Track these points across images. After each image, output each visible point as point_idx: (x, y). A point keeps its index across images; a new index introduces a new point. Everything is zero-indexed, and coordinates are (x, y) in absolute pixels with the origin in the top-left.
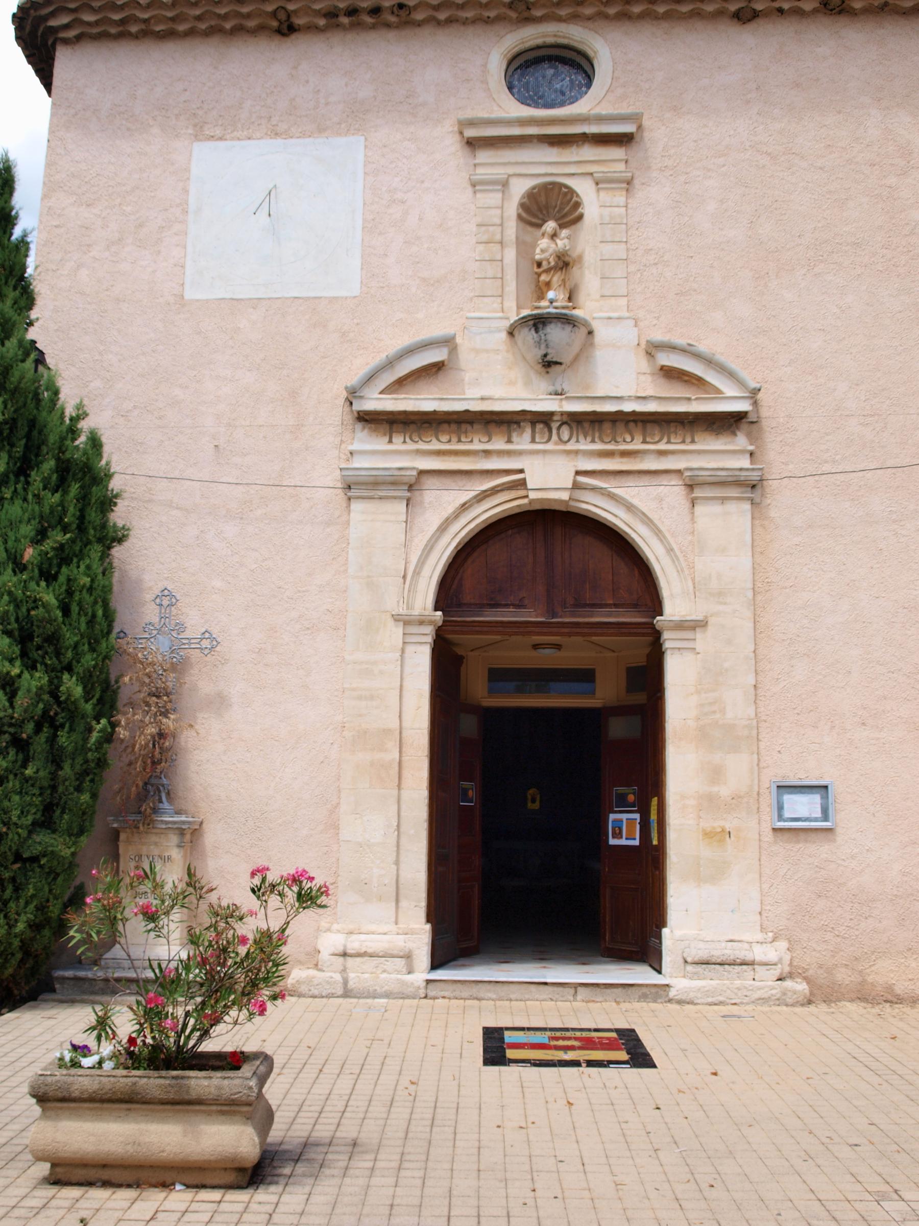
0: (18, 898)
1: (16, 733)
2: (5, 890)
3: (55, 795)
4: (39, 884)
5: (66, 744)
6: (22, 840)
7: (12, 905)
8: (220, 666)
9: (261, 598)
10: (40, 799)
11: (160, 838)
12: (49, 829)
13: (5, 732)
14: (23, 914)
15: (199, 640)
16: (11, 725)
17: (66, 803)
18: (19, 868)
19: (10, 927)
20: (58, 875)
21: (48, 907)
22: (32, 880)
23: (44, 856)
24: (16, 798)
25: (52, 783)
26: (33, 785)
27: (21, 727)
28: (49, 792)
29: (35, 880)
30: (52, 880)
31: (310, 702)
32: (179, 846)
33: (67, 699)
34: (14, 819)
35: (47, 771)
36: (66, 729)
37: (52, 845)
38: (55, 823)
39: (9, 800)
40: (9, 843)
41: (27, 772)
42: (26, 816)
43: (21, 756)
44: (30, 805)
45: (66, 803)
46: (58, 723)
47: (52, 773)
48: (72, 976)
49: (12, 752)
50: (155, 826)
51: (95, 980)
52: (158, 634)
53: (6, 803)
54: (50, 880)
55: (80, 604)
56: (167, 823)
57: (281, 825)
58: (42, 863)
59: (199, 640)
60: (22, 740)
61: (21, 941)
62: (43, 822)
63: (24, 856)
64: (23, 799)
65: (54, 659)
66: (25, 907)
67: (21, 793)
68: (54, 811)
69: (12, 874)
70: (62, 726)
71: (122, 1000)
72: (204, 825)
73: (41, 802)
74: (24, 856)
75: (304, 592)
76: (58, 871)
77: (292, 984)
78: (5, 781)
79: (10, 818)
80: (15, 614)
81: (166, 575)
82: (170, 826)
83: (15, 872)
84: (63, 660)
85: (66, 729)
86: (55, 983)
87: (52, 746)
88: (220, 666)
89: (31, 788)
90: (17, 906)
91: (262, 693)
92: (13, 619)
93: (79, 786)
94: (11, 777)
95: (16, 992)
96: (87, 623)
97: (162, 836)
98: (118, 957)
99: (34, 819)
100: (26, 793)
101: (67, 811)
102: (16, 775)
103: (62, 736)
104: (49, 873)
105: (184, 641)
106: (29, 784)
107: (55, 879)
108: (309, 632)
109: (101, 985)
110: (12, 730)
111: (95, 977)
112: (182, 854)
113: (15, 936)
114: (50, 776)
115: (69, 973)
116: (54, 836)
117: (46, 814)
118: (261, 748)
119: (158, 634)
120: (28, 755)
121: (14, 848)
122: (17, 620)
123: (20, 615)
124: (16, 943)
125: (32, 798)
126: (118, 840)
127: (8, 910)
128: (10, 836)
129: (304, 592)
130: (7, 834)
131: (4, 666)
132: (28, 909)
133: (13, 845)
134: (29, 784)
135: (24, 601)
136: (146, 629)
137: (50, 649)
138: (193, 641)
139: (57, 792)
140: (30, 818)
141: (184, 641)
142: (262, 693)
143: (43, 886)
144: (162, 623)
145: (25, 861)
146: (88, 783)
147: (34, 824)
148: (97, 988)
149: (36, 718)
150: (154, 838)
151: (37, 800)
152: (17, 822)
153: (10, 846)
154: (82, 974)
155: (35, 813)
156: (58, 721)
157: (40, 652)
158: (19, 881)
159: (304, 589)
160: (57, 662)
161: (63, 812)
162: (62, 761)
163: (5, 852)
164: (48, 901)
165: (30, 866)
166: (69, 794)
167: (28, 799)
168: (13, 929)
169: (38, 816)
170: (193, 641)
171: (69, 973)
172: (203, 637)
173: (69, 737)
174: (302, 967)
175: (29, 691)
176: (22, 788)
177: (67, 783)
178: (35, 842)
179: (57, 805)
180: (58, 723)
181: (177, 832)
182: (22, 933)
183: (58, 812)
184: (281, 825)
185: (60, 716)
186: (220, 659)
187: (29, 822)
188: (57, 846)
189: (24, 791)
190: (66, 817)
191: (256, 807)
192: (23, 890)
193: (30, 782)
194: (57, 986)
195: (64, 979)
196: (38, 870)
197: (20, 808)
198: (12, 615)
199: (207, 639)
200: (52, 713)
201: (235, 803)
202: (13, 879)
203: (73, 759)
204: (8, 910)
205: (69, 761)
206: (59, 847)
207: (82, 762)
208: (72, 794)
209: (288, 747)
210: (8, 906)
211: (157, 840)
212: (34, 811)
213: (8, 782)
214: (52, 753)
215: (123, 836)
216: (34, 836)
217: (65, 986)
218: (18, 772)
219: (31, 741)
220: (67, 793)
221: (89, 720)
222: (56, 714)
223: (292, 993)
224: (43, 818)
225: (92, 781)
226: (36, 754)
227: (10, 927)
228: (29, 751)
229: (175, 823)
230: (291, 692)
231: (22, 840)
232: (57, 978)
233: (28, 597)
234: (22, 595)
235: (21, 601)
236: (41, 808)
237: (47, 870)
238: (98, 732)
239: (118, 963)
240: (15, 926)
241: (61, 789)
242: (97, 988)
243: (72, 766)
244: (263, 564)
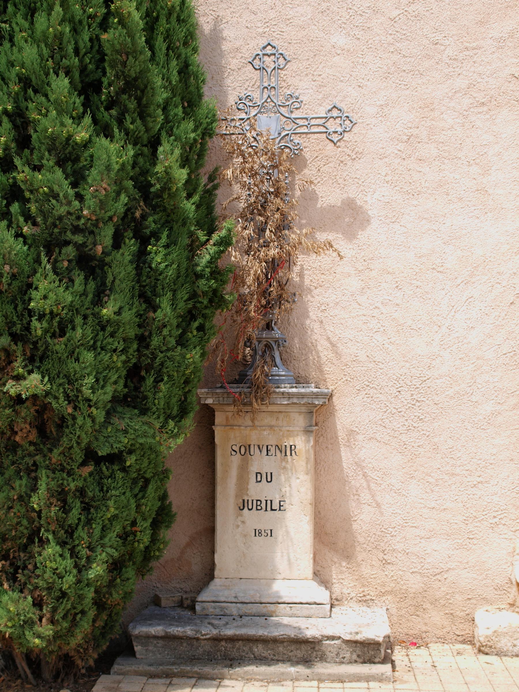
0: (89, 522)
1: (84, 244)
2: (71, 510)
3: (146, 352)
4: (123, 497)
5: (163, 265)
6: (97, 427)
7: (81, 533)
8: (349, 163)
9: (409, 60)
10: (123, 357)
11: (277, 419)
12: (135, 408)
13: (67, 243)
14: (99, 549)
15: (323, 121)
16: (76, 230)
17: (162, 364)
18: (91, 474)
19: (80, 569)
20: (147, 482)
21: (134, 534)
22: (113, 492)
23: (130, 452)
24: (89, 356)
25: (139, 331)
26: (112, 335)
27: (92, 232)
28: (135, 346)
29: (117, 493)
30: (140, 491)
31: (489, 214)
32: (307, 431)
33: (163, 189)
34: (87, 392)
35: (134, 310)
36: (164, 240)
37: (145, 435)
38: (145, 398)
39: (77, 360)
40: (78, 433)
41: (105, 311)
42: (103, 387)
43: (92, 285)
44: (108, 368)
45: (162, 364)
46: (148, 231)
47: (141, 316)
48: (162, 634)
49: (79, 279)
50: (272, 400)
51: (198, 639)
52: (260, 112)
53: (72, 366)
54: (137, 490)
55: (168, 37)
56: (290, 396)
57: (452, 398)
58: (128, 464)
59: (323, 121)
60: (93, 258)
61: (96, 592)
62: (126, 396)
63: (100, 454)
64: (99, 358)
65: (138, 121)
66: (102, 538)
67: (94, 347)
68: (143, 379)
69: (80, 484)
70: (155, 235)
71: (246, 672)
72: (334, 399)
73: (124, 362)
74: (100, 454)
75: (475, 49)
76: (148, 475)
77: (487, 637)
78: (70, 326)
79: (79, 391)
80: (73, 42)
81: (261, 30)
82: (295, 400)
83: (85, 480)
84: (151, 125)
85: (164, 240)
86: (135, 644)
87: (138, 269)
88: (349, 163)
89: (111, 340)
90: (90, 535)
91: (415, 202)
92: (70, 49)
93: (181, 336)
94: (79, 320)
95: (79, 662)
96: (179, 73)
97: (281, 416)
98: (223, 599)
99: (115, 391)
100: (102, 348)
101: (166, 378)
102: (85, 317)
103: (156, 253)
104: (135, 481)
105: (301, 122)
106: (107, 334)
107: (144, 488)
108: (485, 109)
109: (207, 646)
110: (79, 239)
111: (199, 635)
112: (312, 443)
113: (88, 585)
114: (137, 320)
115: (157, 630)
116: (145, 418)
117: (129, 383)
118: (419, 283)
119: (260, 112)
120: (104, 284)
121: (85, 441)
122: (77, 51)
123: (81, 45)
124: (90, 594)
125: (111, 356)
126: (214, 424)
127: (77, 542)
128: (80, 421)
129: (475, 49)
130: (74, 418)
131: (62, 124)
132: (107, 540)
133: (84, 436)
134: (107, 334)
135: (85, 23)
136: (241, 106)
137: (132, 105)
138: (313, 122)
139: (147, 347)
140: (109, 389)
141: (301, 122)
142: (415, 202)
143: (128, 501)
144: (265, 96)
145: (98, 460)
146: (195, 333)
147: (115, 400)
148: (201, 650)
149: (115, 219)
150: (268, 420)
151: (119, 360)
152: (91, 397)
153: (79, 437)
154: (176, 630)
155: (115, 383)
156: (147, 228)
157: (114, 112)
158: (90, 494)
159: (475, 45)
160: (143, 128)
161: (158, 380)
162: (156, 295)
163: (72, 447)
164: (134, 523)
165: (107, 468)
166: (168, 350)
167: (107, 358)
168: (84, 573)
169: (120, 387)
170: (313, 122)
171: (157, 630)
172: (329, 115)
173: (168, 254)
174: (489, 608)
175: (108, 168)
176: (95, 338)
177: (165, 332)
178: (117, 430)
179: (149, 368)
180: (148, 231)
181: (304, 409)
182: (98, 577)
183: (150, 381)
184: (452, 398)
185: (151, 219)
186: (350, 153)
187: (108, 397)
188: (154, 437)
189: (99, 344)
190: (162, 386)
191: (413, 371)
192: (97, 508)
193: (109, 329)
194: (138, 648)
195: (148, 637)
196: (120, 475)
197: (94, 374)
198: (69, 42)
199: (335, 118)
200: (138, 214)
201: (382, 366)
202: (81, 492)
203: (174, 291)
204: (77, 542)
205: (169, 294)
206: (158, 438)
207: (186, 297)
208: (173, 349)
209: (459, 281)
210: (76, 535)
211: (274, 423)
212: (114, 378)
213: (73, 329)
214: (138, 281)
215: (219, 418)
216: (115, 420)
217: (150, 648)
218: (89, 312)
219: (107, 259)
220: (164, 348)
221: (193, 228)
222: (144, 217)
223: (487, 650)
224: (126, 390)
225: (201, 328)
226: (117, 282)
227: (80, 569)
228: (104, 277)
229: (302, 396)
230: (460, 199)
231: (97, 427)
232: (137, 637)
233: (90, 17)
234: (81, 12)
235: (80, 22)
236: (125, 373)
237: (135, 475)
238: (214, 245)
239: (222, 608)
240: (88, 567)
241: (155, 341)
242: (201, 650)
243: (174, 305)
244: (410, 9)
